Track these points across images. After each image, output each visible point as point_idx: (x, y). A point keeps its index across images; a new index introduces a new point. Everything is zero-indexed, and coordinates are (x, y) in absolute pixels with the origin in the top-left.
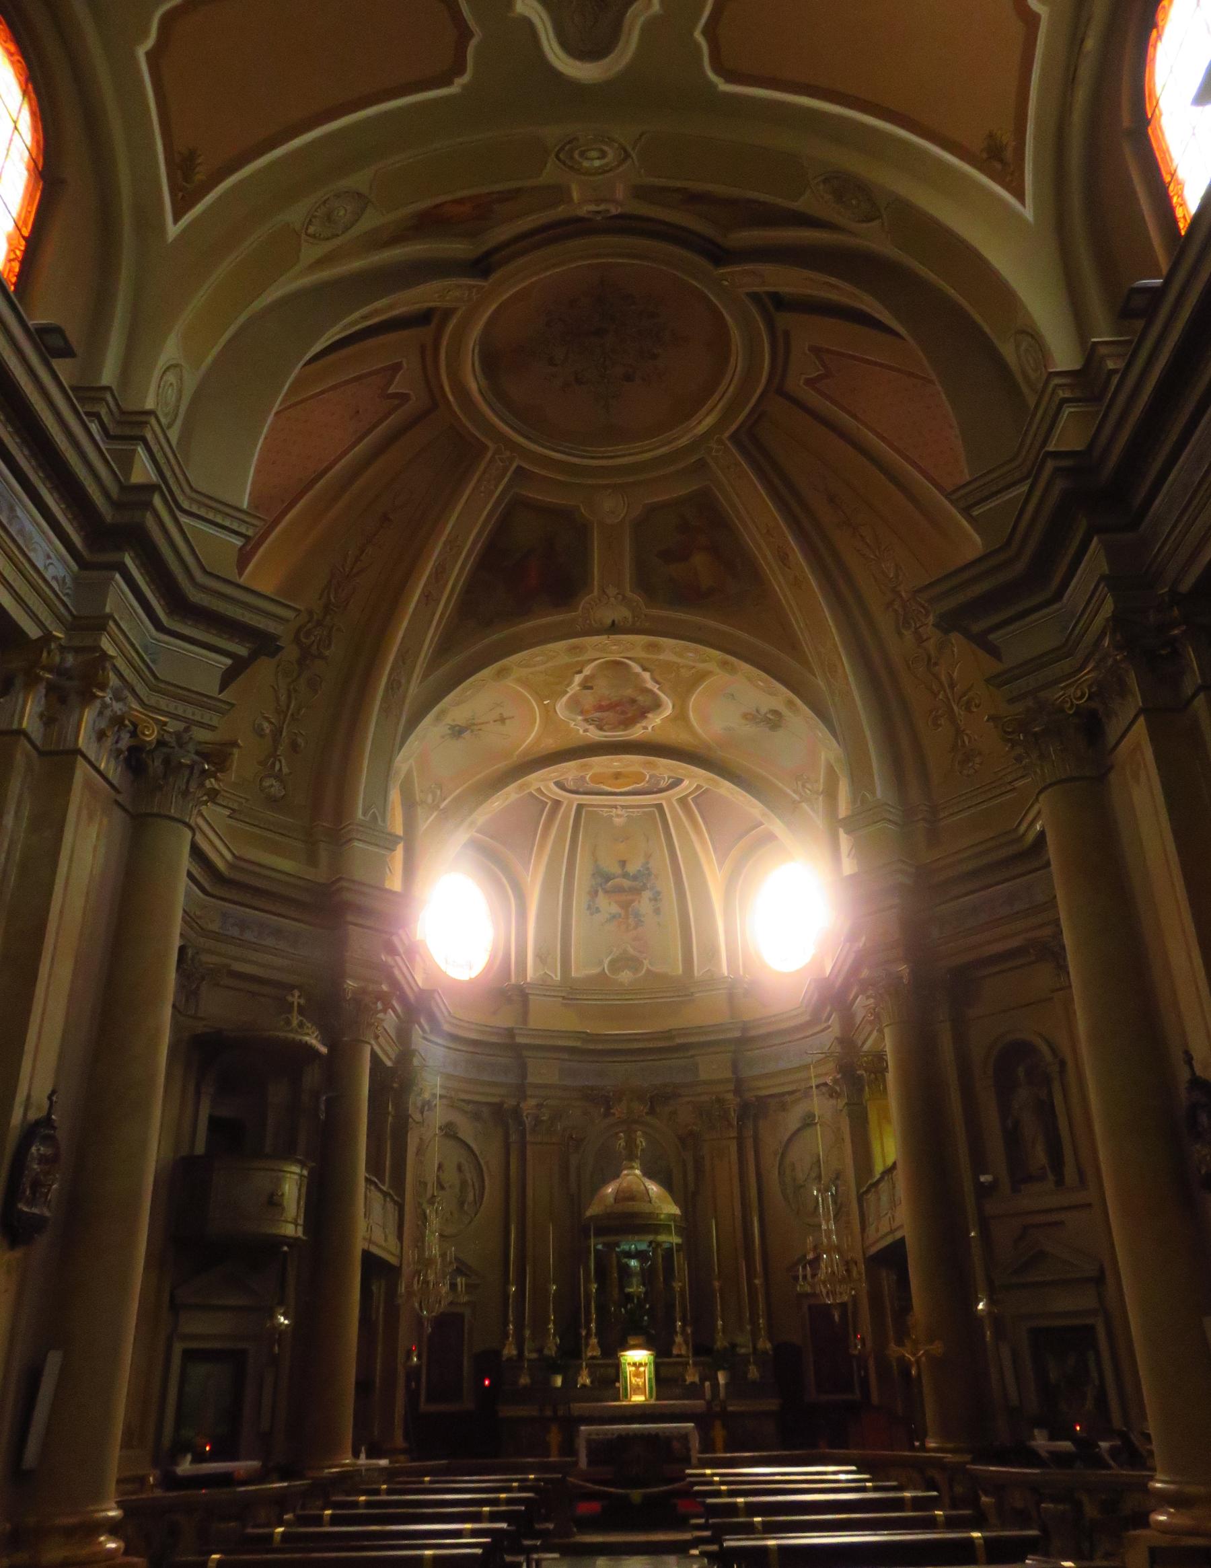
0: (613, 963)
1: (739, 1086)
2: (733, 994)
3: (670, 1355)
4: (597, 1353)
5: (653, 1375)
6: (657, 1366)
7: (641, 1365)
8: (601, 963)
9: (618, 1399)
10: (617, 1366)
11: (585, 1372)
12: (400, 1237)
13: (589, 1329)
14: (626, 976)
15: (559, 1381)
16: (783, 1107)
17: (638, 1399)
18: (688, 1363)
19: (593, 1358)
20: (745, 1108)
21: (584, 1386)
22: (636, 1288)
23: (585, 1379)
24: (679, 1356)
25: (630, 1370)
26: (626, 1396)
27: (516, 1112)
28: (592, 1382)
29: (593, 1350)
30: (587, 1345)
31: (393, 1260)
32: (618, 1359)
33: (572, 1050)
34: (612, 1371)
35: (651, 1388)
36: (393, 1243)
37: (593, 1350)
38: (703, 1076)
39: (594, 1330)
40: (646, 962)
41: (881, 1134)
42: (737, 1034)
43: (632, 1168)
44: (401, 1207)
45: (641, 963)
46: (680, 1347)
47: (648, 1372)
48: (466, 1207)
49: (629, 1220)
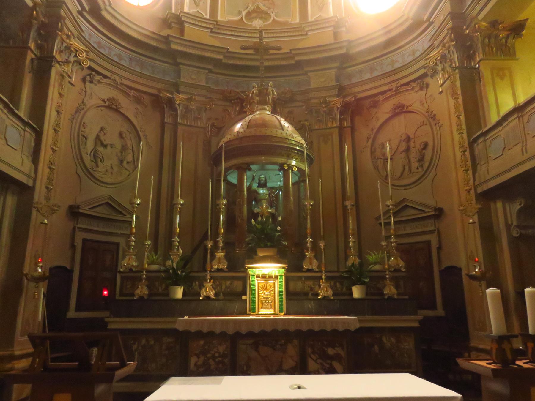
0: (248, 14)
1: (341, 90)
2: (337, 26)
3: (299, 269)
4: (224, 265)
5: (283, 289)
6: (288, 280)
7: (270, 277)
8: (240, 13)
9: (245, 314)
10: (245, 279)
11: (208, 285)
12: (35, 160)
13: (216, 243)
14: (257, 23)
15: (179, 293)
16: (376, 105)
17: (266, 312)
18: (320, 278)
19: (219, 270)
20: (345, 108)
21: (208, 298)
22: (264, 208)
23: (208, 291)
24: (309, 270)
25: (256, 282)
26: (254, 309)
27: (171, 102)
28: (216, 295)
29: (219, 261)
30: (213, 256)
31: (30, 184)
32: (245, 271)
33: (217, 63)
34: (237, 285)
35: (281, 302)
36: (28, 166)
37: (219, 261)
38: (313, 85)
39: (221, 244)
40: (273, 15)
41: (495, 90)
42: (343, 51)
43: (265, 109)
44: (38, 134)
45: (270, 16)
46: (310, 262)
47: (279, 286)
48: (125, 164)
49: (261, 147)
